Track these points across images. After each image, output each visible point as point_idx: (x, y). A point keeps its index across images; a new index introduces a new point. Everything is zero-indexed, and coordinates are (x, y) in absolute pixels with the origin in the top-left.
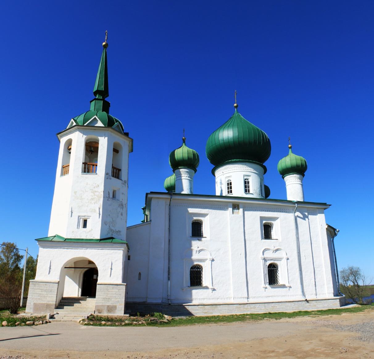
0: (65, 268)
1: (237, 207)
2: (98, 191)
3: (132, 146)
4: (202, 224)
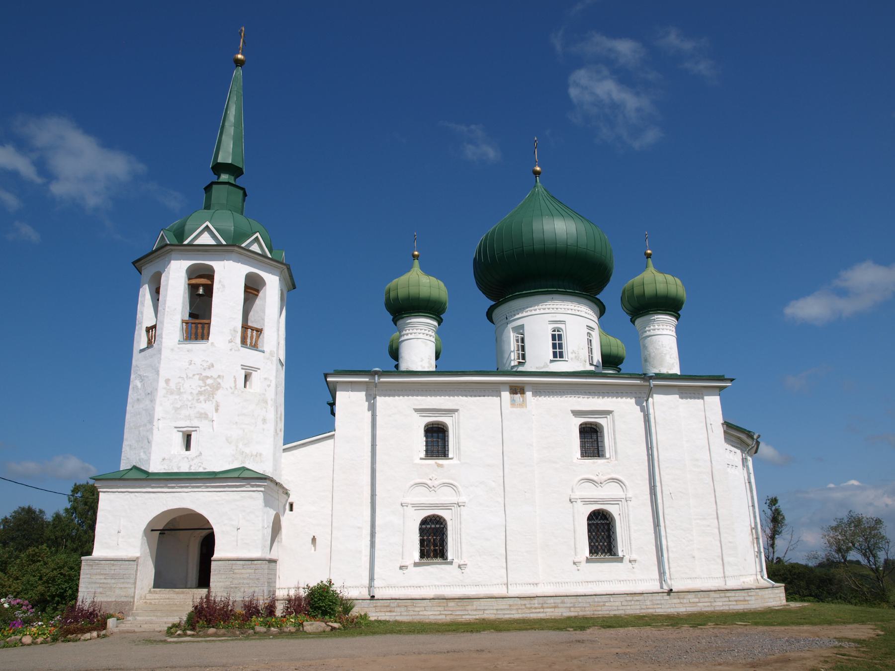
0: (152, 530)
2: (212, 376)
3: (291, 276)
4: (448, 431)
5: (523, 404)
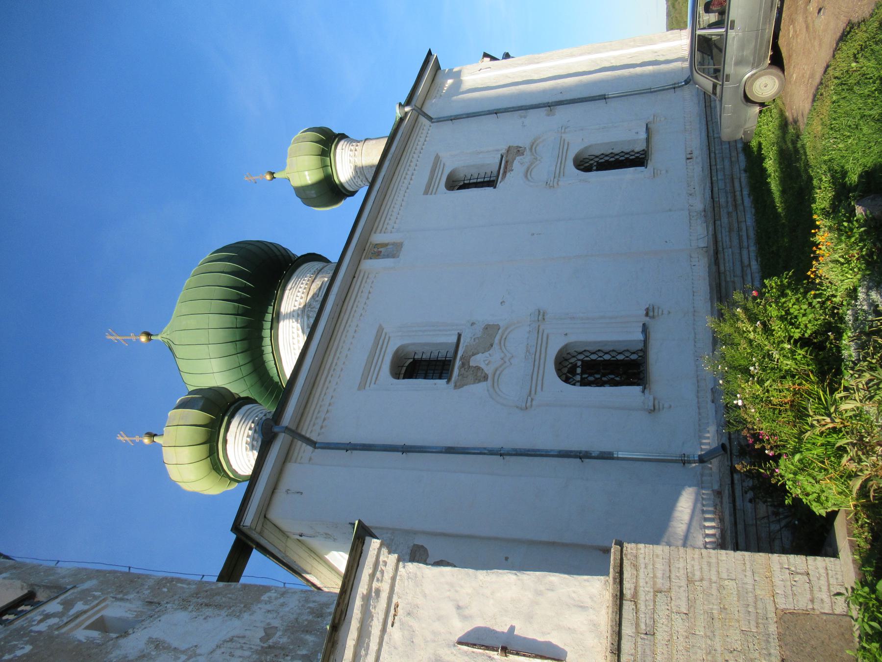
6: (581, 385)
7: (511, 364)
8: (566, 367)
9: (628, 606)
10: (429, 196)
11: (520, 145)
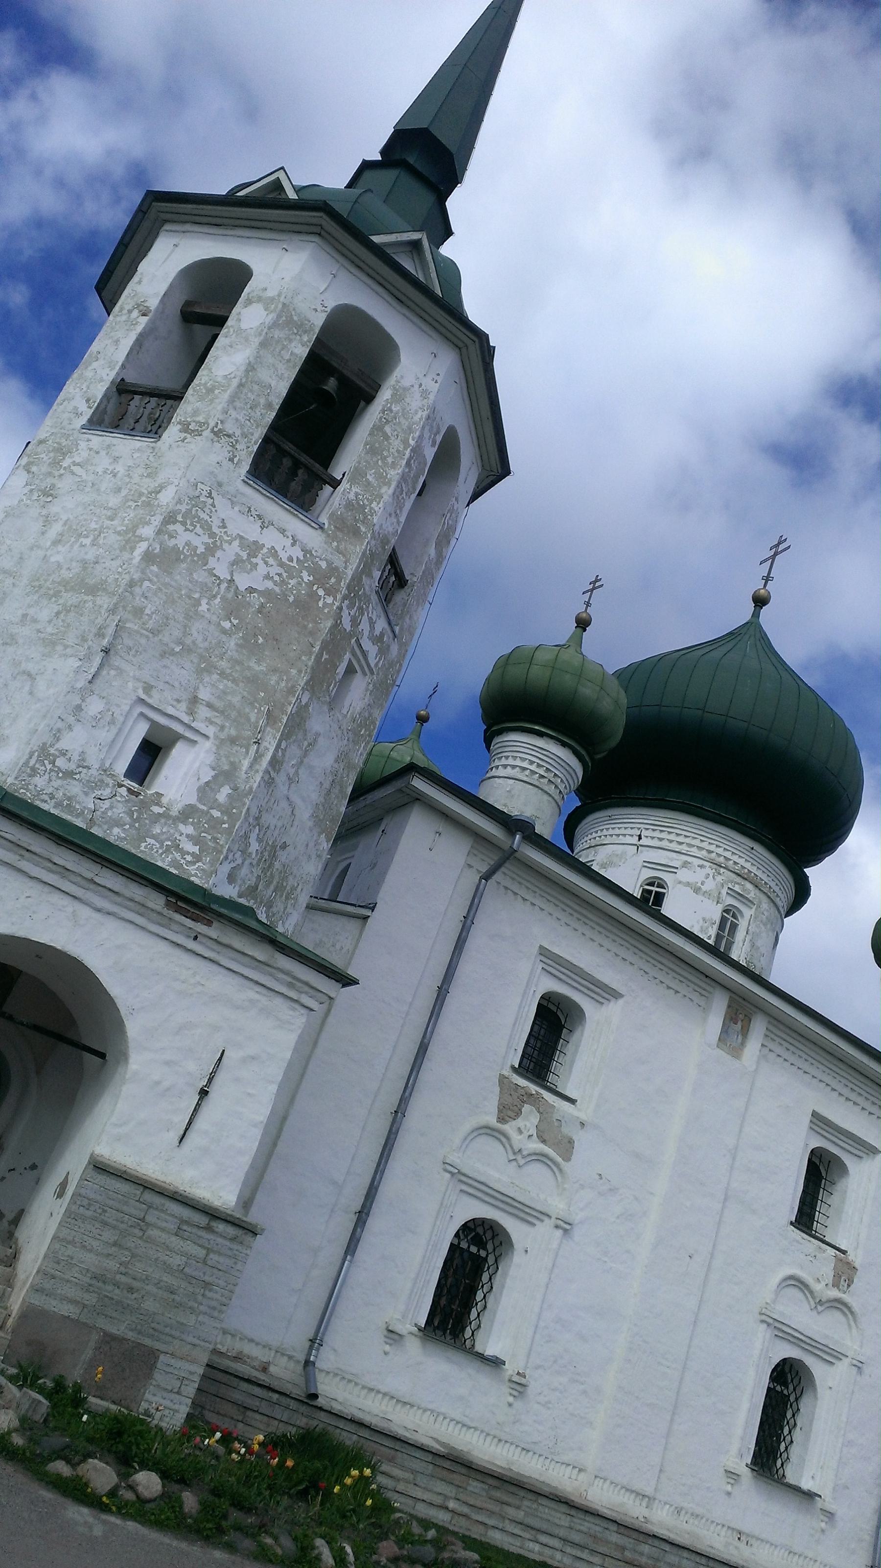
1: (740, 1023)
5: (736, 1052)
6: (452, 1244)
7: (510, 1161)
8: (484, 1234)
9: (203, 1220)
10: (809, 1117)
11: (852, 1286)
